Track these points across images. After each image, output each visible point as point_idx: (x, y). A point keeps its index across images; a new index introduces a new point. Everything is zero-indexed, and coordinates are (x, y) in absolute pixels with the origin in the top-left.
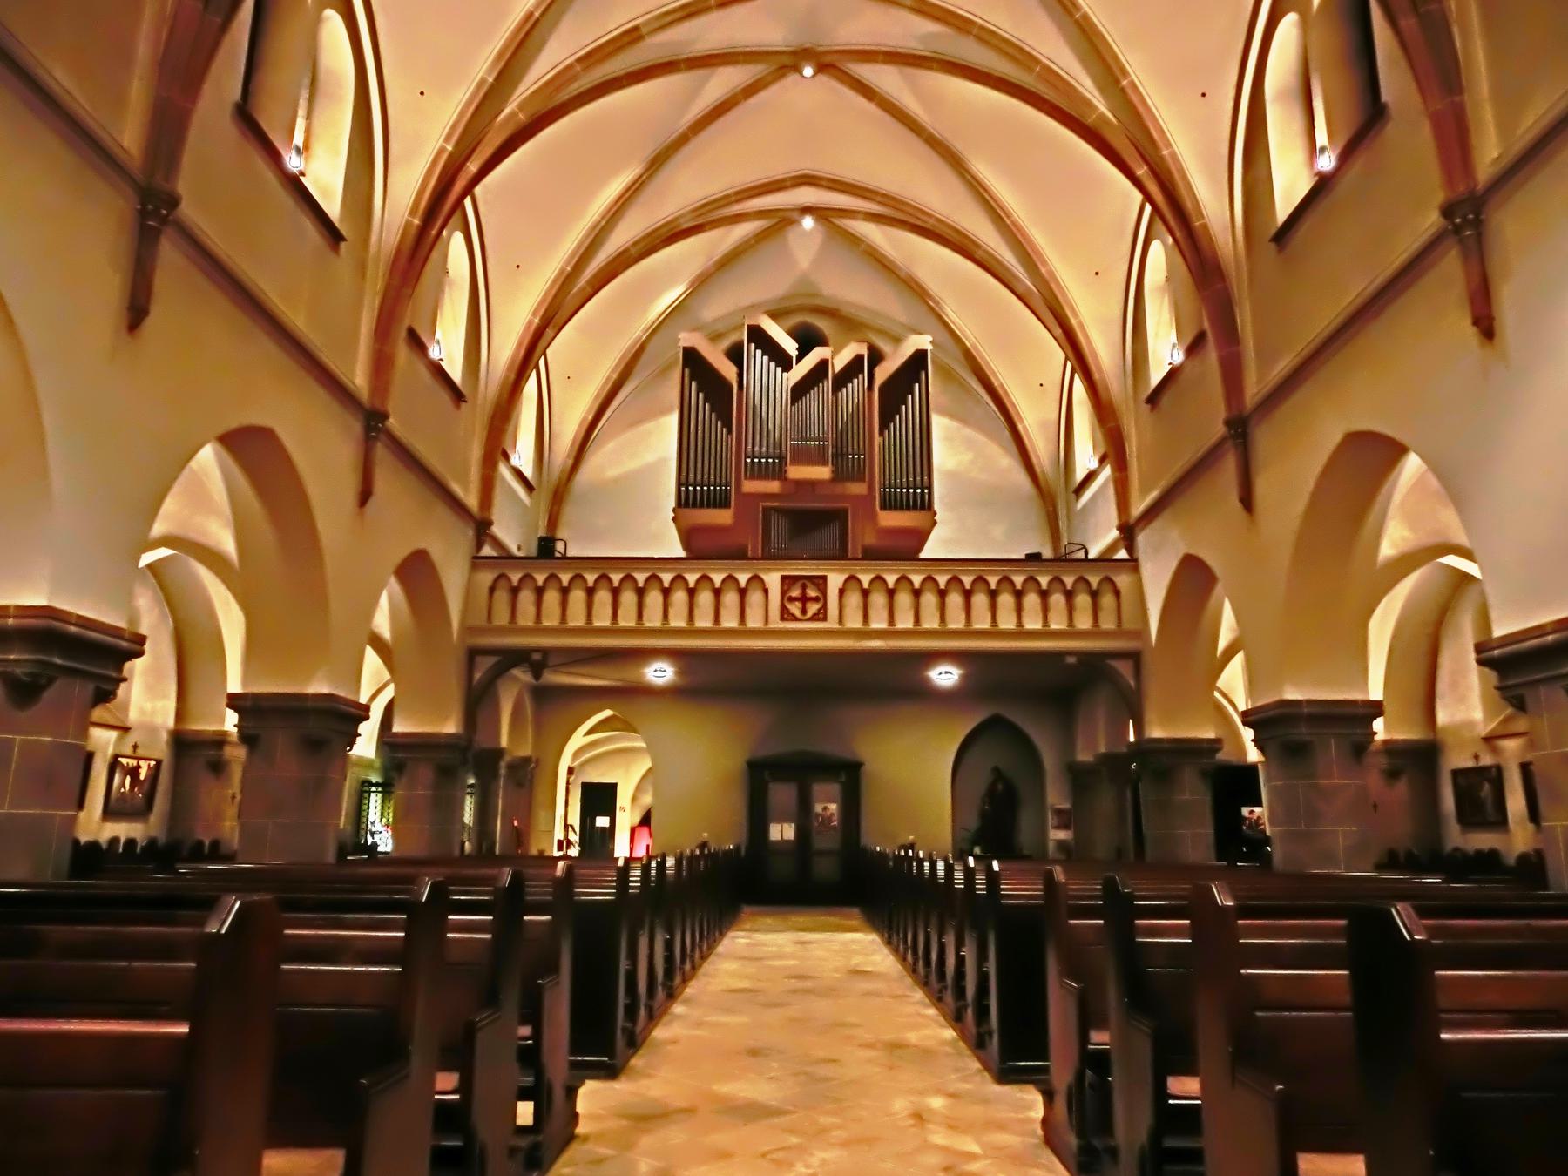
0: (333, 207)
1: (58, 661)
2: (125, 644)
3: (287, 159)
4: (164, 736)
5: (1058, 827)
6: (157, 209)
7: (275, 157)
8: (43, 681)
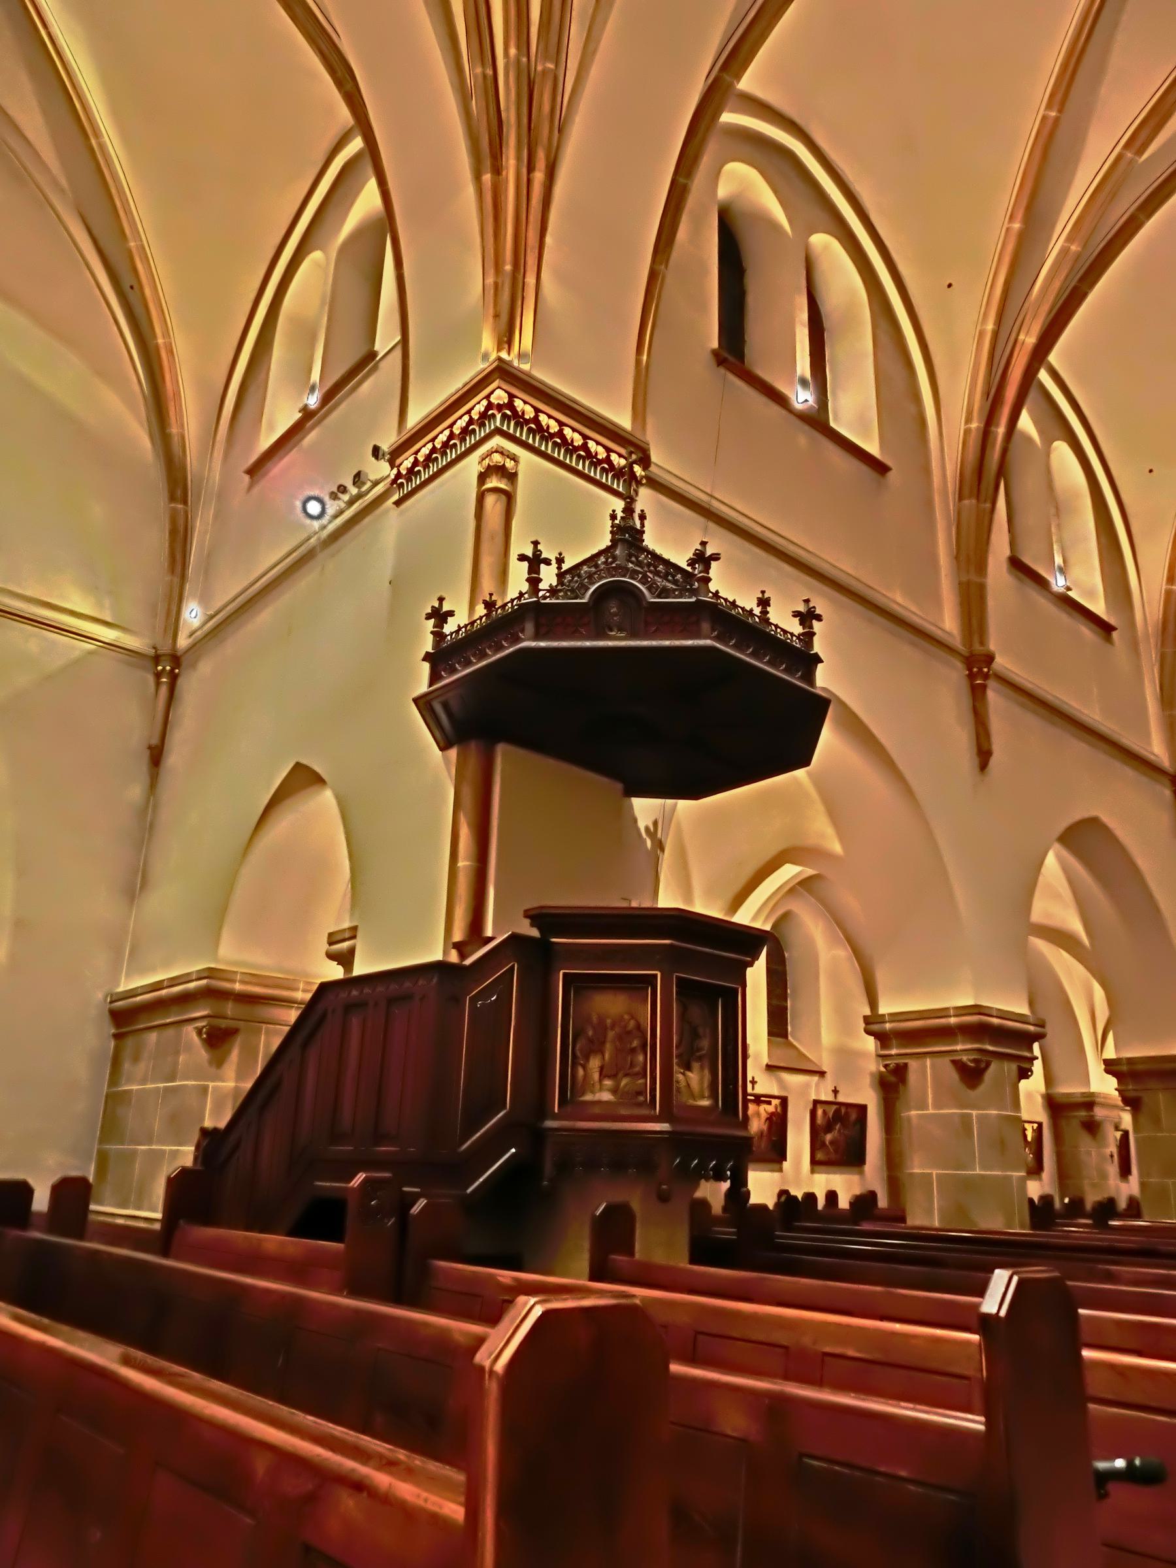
0: (1099, 607)
1: (991, 1048)
2: (1031, 1028)
3: (792, 397)
4: (1039, 1100)
5: (981, 1291)
6: (980, 670)
7: (1041, 582)
8: (983, 1065)
